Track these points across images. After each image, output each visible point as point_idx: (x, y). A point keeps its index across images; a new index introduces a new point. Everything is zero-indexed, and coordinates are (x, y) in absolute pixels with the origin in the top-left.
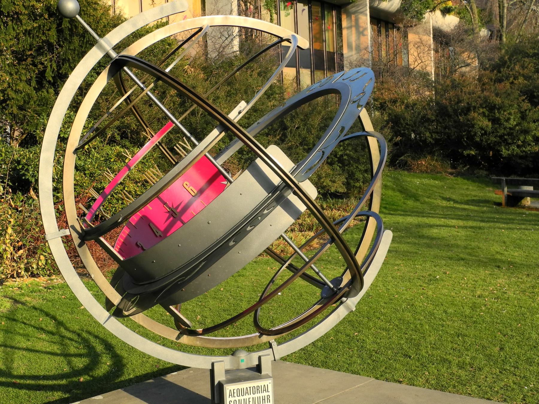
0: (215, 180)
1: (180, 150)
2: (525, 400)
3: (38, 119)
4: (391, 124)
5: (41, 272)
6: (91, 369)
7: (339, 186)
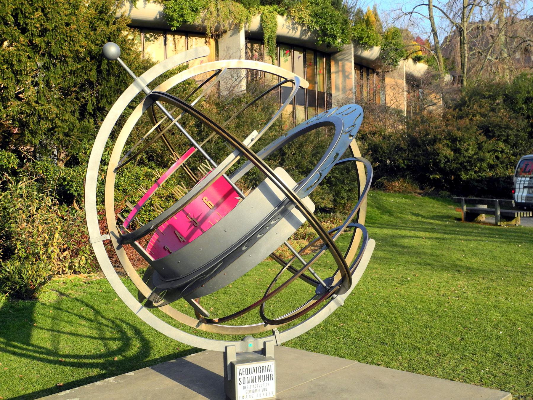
0: (229, 196)
2: (481, 381)
3: (80, 144)
4: (370, 152)
5: (82, 270)
6: (124, 351)
7: (327, 203)
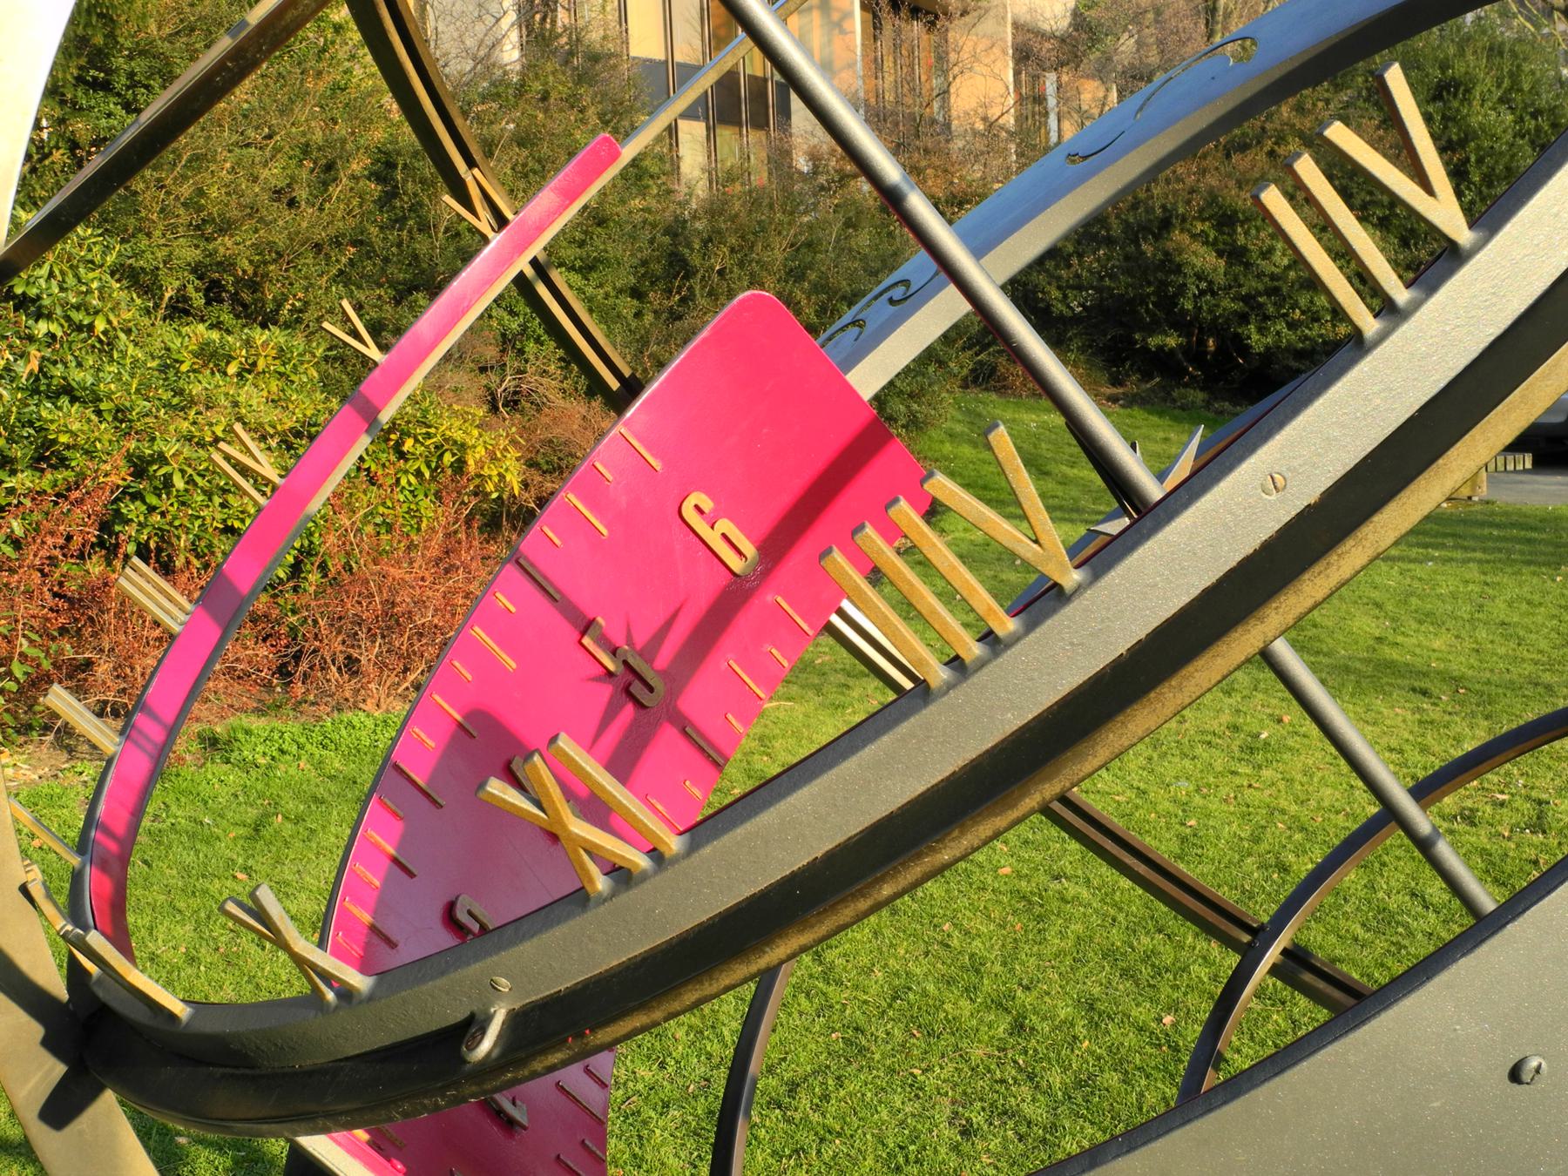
1: (1343, 254)
